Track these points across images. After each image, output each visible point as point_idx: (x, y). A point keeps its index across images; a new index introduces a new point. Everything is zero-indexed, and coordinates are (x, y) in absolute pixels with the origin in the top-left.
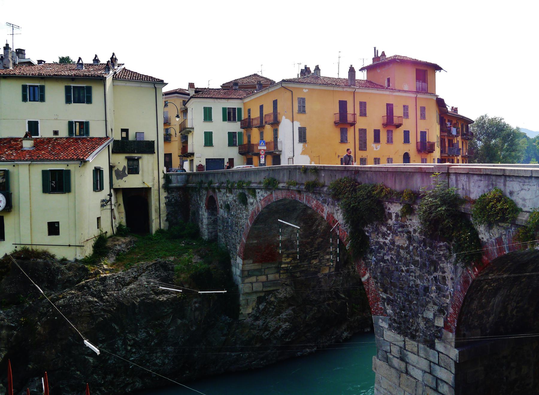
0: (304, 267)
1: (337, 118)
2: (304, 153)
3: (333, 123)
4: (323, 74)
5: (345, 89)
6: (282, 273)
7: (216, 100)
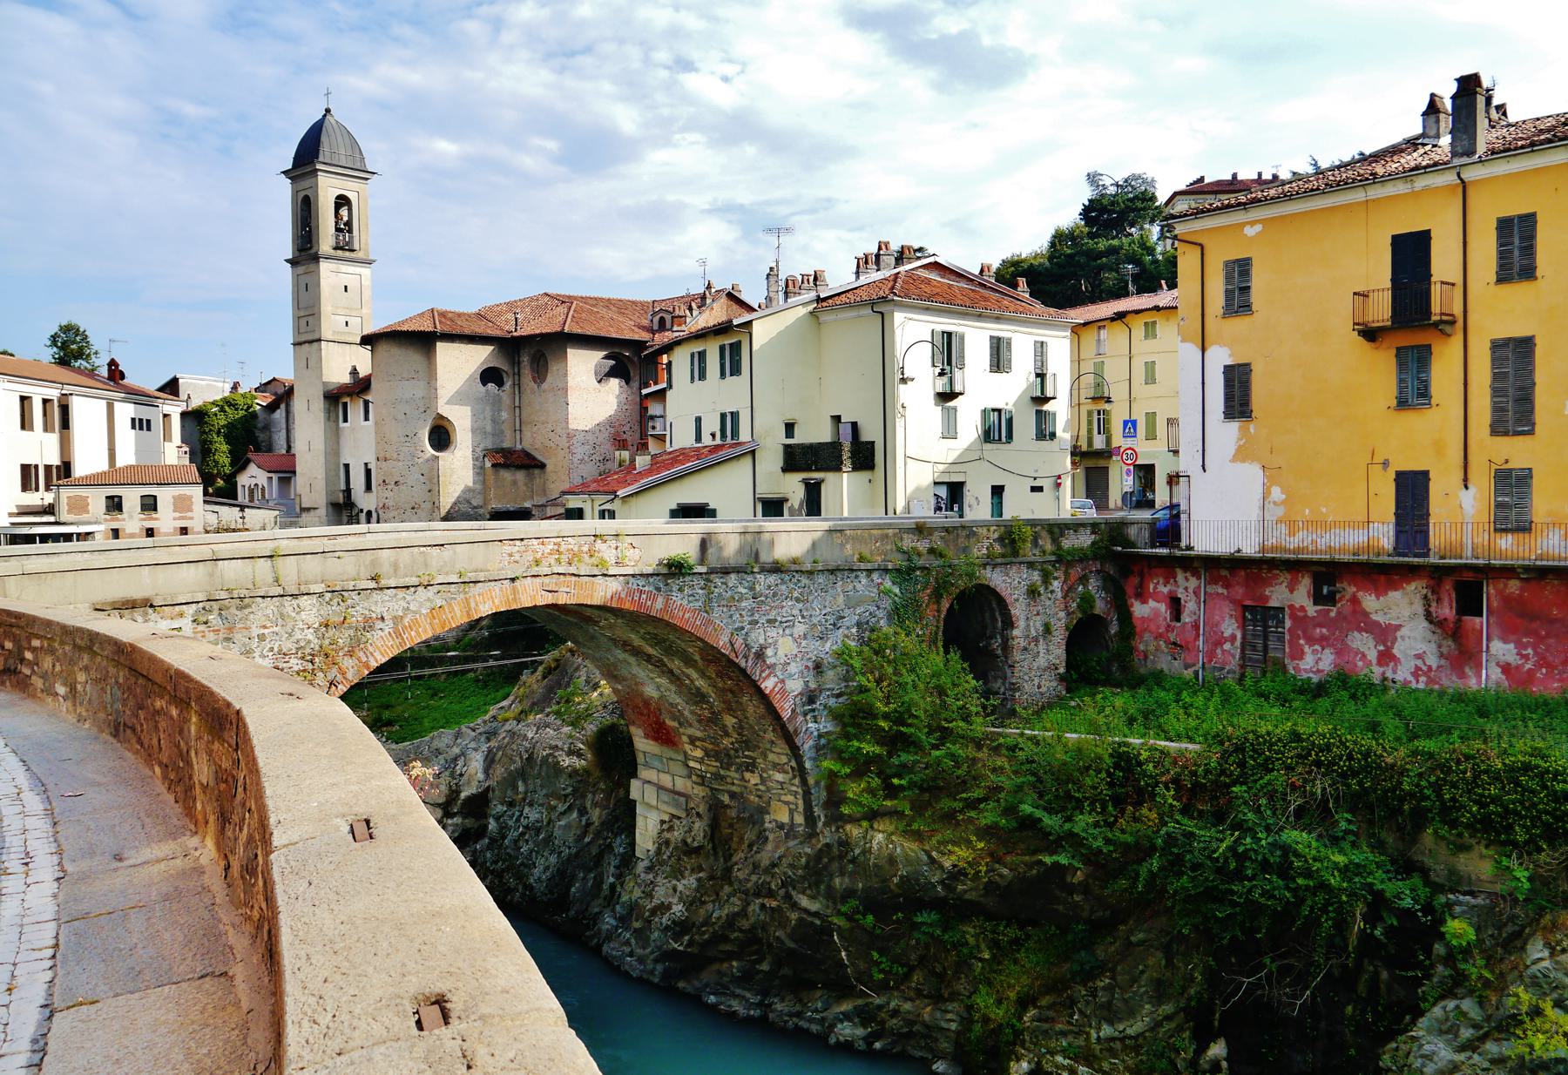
1: (1381, 310)
2: (1241, 455)
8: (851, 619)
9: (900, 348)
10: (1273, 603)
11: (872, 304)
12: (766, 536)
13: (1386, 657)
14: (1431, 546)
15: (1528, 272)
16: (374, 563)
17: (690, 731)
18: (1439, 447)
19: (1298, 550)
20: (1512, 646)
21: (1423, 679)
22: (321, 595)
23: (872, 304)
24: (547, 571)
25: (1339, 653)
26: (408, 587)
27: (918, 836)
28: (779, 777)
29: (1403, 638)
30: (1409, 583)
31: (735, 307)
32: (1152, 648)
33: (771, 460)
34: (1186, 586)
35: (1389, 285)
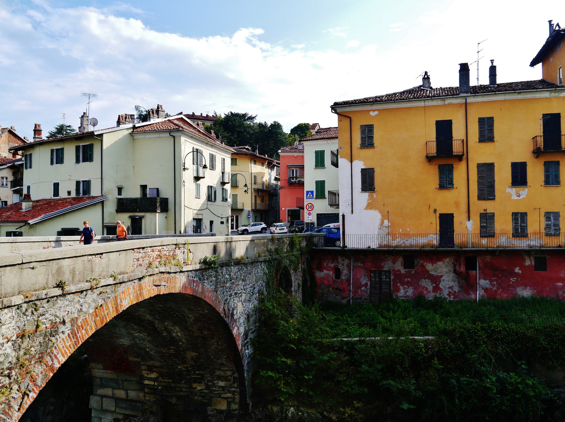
0: (181, 391)
1: (433, 150)
2: (370, 206)
3: (424, 158)
4: (435, 84)
5: (447, 102)
6: (147, 393)
7: (329, 141)
8: (256, 290)
9: (183, 155)
10: (386, 269)
11: (170, 131)
12: (233, 244)
13: (437, 288)
14: (455, 243)
15: (491, 139)
16: (59, 271)
17: (151, 363)
18: (457, 204)
19: (397, 246)
20: (488, 281)
21: (452, 296)
22: (19, 307)
23: (170, 131)
24: (157, 271)
25: (415, 288)
26: (82, 292)
27: (312, 406)
28: (222, 384)
29: (443, 280)
30: (446, 258)
31: (12, 137)
32: (325, 291)
33: (111, 206)
34: (343, 264)
35: (435, 140)
